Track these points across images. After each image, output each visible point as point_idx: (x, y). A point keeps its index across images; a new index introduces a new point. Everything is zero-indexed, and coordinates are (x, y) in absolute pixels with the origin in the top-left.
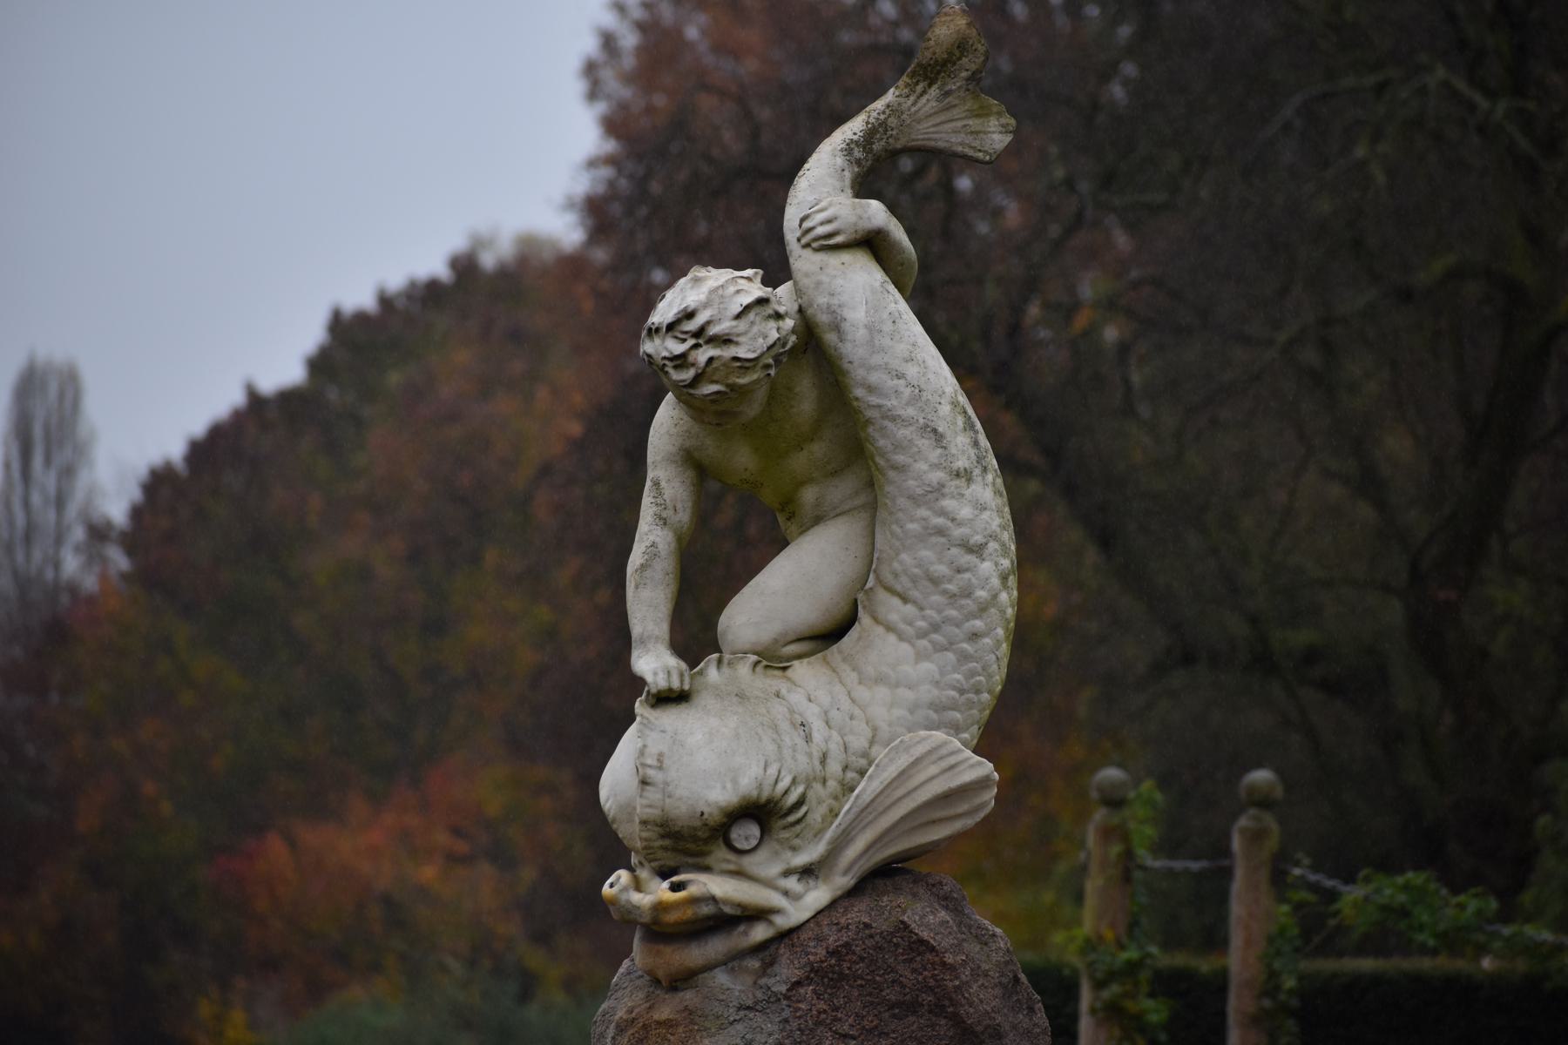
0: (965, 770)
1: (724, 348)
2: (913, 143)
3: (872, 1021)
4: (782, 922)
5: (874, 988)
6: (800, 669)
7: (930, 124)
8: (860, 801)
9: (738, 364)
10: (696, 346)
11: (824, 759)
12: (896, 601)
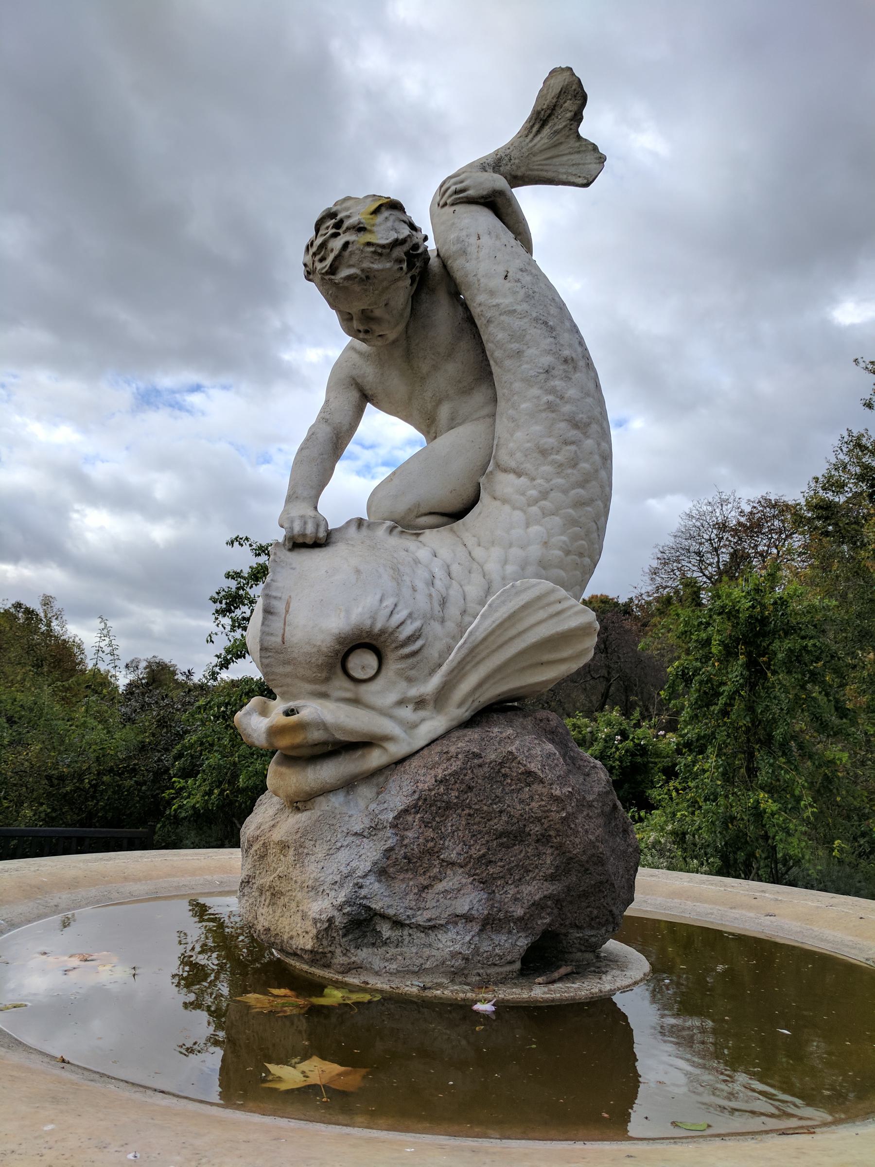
0: (570, 616)
2: (530, 173)
3: (479, 851)
4: (397, 750)
5: (482, 818)
6: (429, 536)
7: (544, 157)
8: (473, 638)
9: (372, 249)
11: (443, 602)
12: (511, 477)
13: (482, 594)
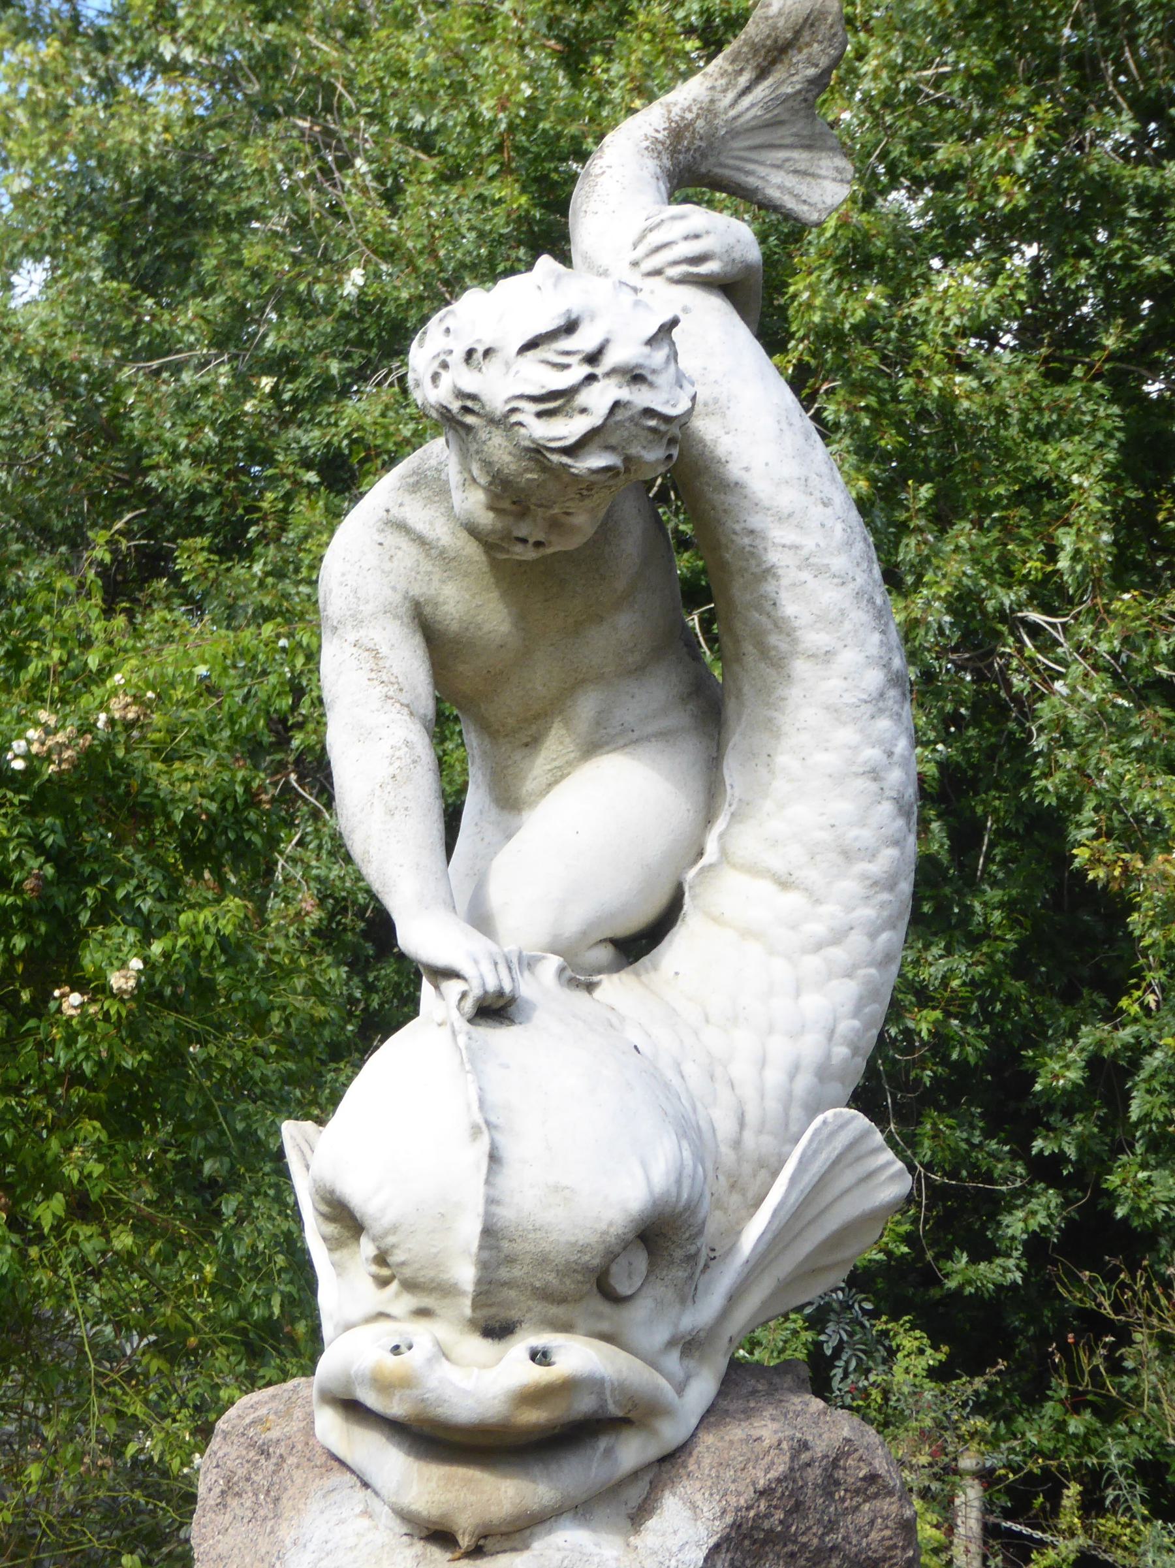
1: (635, 388)
10: (591, 378)
13: (736, 1128)
